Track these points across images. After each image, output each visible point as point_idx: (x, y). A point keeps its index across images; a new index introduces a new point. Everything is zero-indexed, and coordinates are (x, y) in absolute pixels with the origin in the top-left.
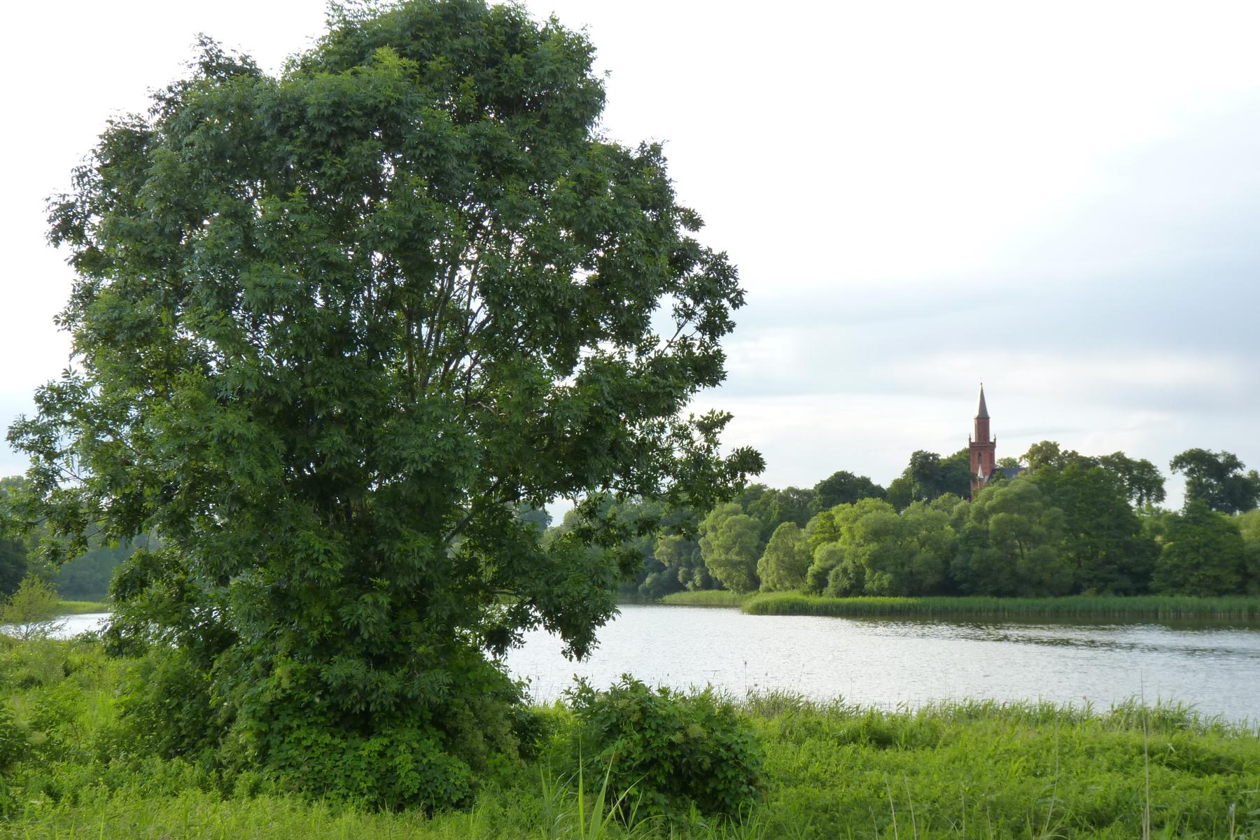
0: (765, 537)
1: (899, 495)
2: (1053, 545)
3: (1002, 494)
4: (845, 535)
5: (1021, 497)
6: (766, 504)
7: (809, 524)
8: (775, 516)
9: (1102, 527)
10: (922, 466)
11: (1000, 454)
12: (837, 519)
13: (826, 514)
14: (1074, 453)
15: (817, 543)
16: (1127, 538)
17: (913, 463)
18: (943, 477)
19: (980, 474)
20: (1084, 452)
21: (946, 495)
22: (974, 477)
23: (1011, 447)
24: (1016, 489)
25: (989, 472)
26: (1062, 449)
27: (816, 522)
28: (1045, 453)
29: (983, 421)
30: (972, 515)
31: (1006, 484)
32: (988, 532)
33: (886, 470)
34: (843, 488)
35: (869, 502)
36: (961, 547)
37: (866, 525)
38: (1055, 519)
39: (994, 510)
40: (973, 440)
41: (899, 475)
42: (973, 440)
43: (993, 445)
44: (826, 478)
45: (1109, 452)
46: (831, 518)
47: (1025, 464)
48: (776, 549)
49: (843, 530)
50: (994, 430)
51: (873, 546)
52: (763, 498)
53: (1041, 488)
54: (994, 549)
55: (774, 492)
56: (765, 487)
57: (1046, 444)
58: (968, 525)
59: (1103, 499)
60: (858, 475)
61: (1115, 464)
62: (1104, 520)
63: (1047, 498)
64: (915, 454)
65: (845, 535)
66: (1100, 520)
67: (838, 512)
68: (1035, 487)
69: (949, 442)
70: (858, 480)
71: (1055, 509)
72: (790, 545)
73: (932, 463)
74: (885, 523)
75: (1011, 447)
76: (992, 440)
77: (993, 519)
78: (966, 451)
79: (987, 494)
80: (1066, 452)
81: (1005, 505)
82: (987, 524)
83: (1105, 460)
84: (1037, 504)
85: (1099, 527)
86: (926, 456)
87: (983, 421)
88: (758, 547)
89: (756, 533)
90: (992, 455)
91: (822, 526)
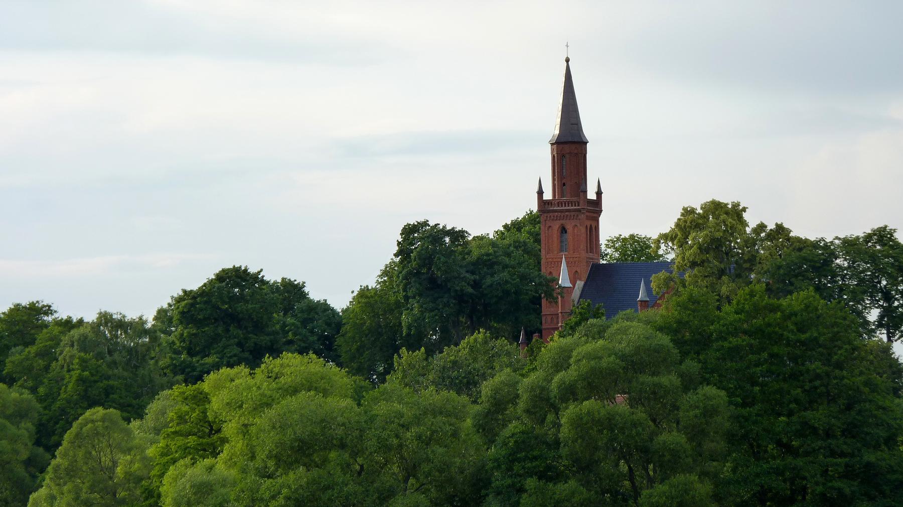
0: (47, 437)
1: (366, 337)
2: (704, 474)
3: (590, 356)
4: (235, 446)
5: (637, 363)
6: (48, 354)
7: (153, 408)
8: (70, 388)
9: (815, 430)
10: (427, 259)
11: (611, 227)
12: (216, 404)
13: (190, 389)
14: (780, 229)
15: (169, 459)
16: (870, 457)
17: (403, 251)
18: (476, 285)
19: (564, 280)
20: (805, 229)
21: (480, 335)
22: (549, 286)
23: (636, 206)
24: (622, 346)
25: (585, 272)
26: (752, 220)
27: (168, 403)
28: (714, 232)
29: (570, 149)
30: (522, 405)
31: (600, 333)
32: (557, 443)
33: (342, 270)
34: (237, 316)
35: (293, 365)
36: (499, 479)
37: (281, 426)
38: (709, 412)
39: (570, 393)
40: (548, 195)
41: (370, 278)
42: (548, 195)
43: (596, 206)
44: (195, 285)
45: (859, 229)
46: (202, 399)
47: (669, 253)
48: (71, 472)
49: (230, 429)
50: (598, 171)
51: (296, 478)
52: (42, 337)
53: (678, 343)
54: (572, 483)
55: (67, 325)
56: (48, 310)
57: (715, 207)
58: (513, 427)
59: (815, 366)
60: (272, 276)
61: (873, 258)
62: (819, 416)
63: (691, 365)
64: (409, 231)
65: (235, 446)
66: (809, 414)
67: (218, 387)
68: (664, 340)
69: (492, 198)
70: (274, 288)
71: (710, 390)
72: (106, 460)
73: (449, 253)
74: (324, 422)
75: (636, 206)
76: (591, 195)
77: (570, 412)
78: (531, 219)
79: (570, 349)
80: (762, 227)
81: (597, 383)
82: (557, 425)
83: (850, 245)
84: (669, 380)
85: (807, 430)
86: (436, 235)
87: (570, 149)
88: (29, 463)
89: (26, 429)
90: (593, 231)
91: (182, 419)
